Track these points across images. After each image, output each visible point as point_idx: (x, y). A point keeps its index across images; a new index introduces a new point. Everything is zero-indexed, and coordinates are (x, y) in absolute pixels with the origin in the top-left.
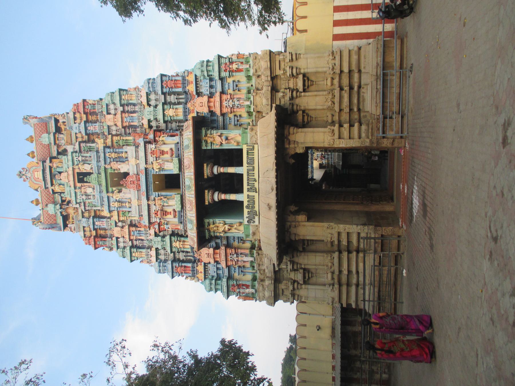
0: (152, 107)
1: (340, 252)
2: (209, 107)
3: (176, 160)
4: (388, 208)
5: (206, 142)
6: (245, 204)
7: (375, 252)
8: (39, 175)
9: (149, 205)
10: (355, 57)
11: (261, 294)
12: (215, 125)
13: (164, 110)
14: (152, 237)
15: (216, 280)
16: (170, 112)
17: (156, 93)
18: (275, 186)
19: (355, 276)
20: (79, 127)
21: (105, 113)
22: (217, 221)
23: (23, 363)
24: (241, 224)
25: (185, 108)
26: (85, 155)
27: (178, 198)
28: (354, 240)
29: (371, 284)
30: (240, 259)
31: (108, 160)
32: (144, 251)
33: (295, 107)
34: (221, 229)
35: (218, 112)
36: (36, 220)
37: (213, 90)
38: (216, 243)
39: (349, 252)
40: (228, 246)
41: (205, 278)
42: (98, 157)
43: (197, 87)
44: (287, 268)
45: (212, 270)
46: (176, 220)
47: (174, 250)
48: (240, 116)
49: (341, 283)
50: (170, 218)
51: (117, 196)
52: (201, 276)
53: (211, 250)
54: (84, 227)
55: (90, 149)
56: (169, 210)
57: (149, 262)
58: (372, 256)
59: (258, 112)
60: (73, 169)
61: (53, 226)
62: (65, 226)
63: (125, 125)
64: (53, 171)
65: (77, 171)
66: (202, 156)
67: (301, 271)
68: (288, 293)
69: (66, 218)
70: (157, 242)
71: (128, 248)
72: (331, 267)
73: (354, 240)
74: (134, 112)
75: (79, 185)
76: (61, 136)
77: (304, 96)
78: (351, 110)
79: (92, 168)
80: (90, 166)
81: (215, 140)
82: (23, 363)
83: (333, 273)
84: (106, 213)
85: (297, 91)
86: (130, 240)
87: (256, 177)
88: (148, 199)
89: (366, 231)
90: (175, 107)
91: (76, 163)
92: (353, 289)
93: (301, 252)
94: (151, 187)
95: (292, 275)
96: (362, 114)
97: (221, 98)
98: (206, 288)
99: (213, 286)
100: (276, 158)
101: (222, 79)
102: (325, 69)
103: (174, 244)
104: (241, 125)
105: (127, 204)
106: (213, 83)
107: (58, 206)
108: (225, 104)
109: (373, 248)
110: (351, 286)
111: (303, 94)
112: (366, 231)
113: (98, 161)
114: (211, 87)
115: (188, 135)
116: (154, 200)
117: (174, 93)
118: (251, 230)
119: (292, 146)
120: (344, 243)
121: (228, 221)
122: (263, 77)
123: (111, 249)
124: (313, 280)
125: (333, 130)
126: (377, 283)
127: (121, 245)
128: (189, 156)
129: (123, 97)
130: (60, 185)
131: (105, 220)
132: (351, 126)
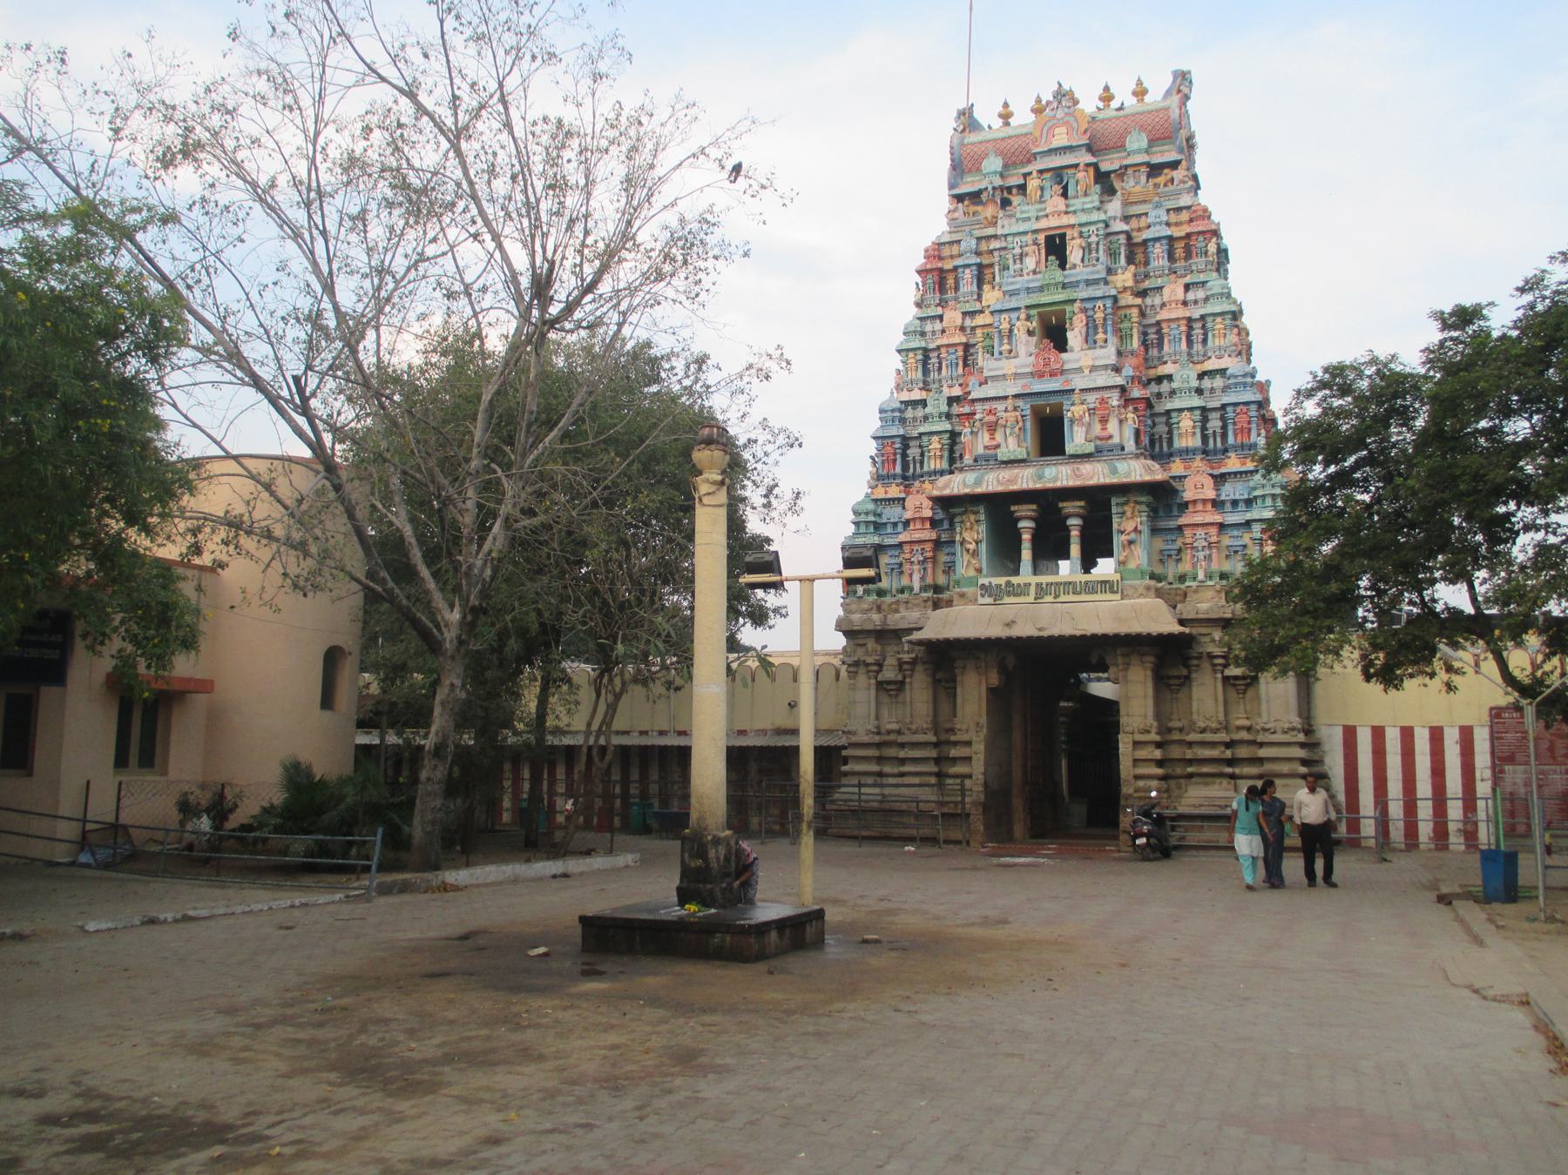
0: (1195, 384)
1: (936, 745)
2: (1195, 502)
3: (1090, 448)
4: (1019, 829)
5: (1126, 503)
6: (1015, 580)
7: (941, 804)
8: (1060, 139)
9: (1006, 398)
11: (854, 607)
12: (1161, 513)
13: (1191, 409)
14: (947, 392)
15: (875, 523)
16: (1186, 423)
17: (1225, 389)
18: (1045, 634)
19: (896, 770)
21: (1188, 279)
22: (983, 528)
23: (788, 363)
24: (979, 571)
25: (1194, 451)
26: (1101, 247)
27: (1021, 453)
28: (959, 769)
29: (883, 795)
30: (916, 567)
31: (1089, 305)
32: (920, 374)
33: (1195, 662)
34: (967, 536)
35: (1183, 521)
36: (967, 122)
37: (1228, 507)
38: (941, 521)
39: (937, 761)
40: (938, 544)
41: (876, 501)
42: (1095, 282)
43: (1235, 473)
45: (892, 513)
46: (980, 451)
47: (925, 439)
48: (1179, 560)
49: (884, 746)
50: (984, 438)
51: (1021, 327)
52: (880, 493)
53: (928, 513)
54: (959, 242)
55: (1113, 254)
56: (999, 436)
57: (899, 388)
58: (934, 798)
59: (1185, 595)
60: (1073, 226)
61: (959, 167)
62: (959, 198)
63: (1164, 325)
64: (1070, 171)
65: (1069, 233)
66: (1098, 500)
67: (900, 678)
68: (860, 654)
69: (975, 197)
70: (937, 405)
71: (923, 344)
73: (959, 769)
74: (1190, 343)
75: (1041, 238)
76: (1143, 178)
78: (1190, 762)
79: (1074, 266)
80: (1078, 261)
81: (1128, 522)
82: (788, 363)
83: (899, 732)
84: (991, 297)
85: (1226, 666)
86: (938, 348)
87: (1062, 598)
88: (1016, 396)
89: (976, 788)
90: (1198, 430)
91: (1085, 229)
92: (875, 768)
93: (934, 676)
94: (1040, 402)
95: (890, 661)
96: (1182, 781)
97: (1212, 524)
98: (859, 503)
99: (863, 518)
100: (1094, 636)
102: (1265, 715)
103: (935, 438)
105: (1006, 347)
106: (1242, 507)
107: (998, 182)
108: (1200, 532)
109: (947, 799)
111: (1219, 675)
112: (976, 788)
113: (1089, 283)
114: (1235, 503)
115: (1136, 470)
116: (1015, 409)
117: (1224, 427)
118: (969, 590)
119: (1120, 660)
120: (954, 753)
121: (983, 547)
123: (919, 305)
124: (885, 698)
125: (1148, 732)
126: (886, 806)
127: (928, 327)
128: (1096, 474)
129: (1219, 319)
130: (1042, 189)
131: (975, 288)
132: (1160, 763)
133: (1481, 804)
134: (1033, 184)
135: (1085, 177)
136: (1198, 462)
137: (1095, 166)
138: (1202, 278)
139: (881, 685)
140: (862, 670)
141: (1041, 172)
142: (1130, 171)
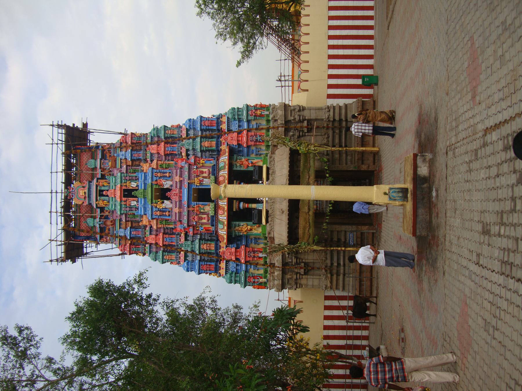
2: (238, 141)
10: (343, 111)
15: (235, 273)
19: (342, 268)
20: (125, 154)
43: (228, 126)
44: (292, 261)
52: (223, 271)
57: (179, 263)
72: (325, 261)
77: (308, 135)
79: (137, 186)
92: (341, 277)
99: (233, 279)
101: (249, 121)
104: (260, 155)
105: (167, 213)
110: (340, 275)
111: (307, 134)
122: (279, 121)
123: (144, 254)
133: (349, 324)
134: (101, 204)
135: (102, 182)
136: (222, 139)
137: (98, 179)
138: (149, 155)
139: (306, 273)
140: (299, 281)
141: (97, 200)
142: (102, 166)
